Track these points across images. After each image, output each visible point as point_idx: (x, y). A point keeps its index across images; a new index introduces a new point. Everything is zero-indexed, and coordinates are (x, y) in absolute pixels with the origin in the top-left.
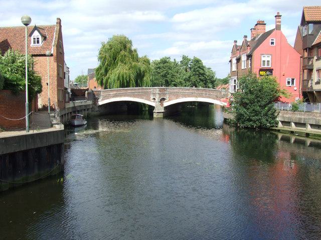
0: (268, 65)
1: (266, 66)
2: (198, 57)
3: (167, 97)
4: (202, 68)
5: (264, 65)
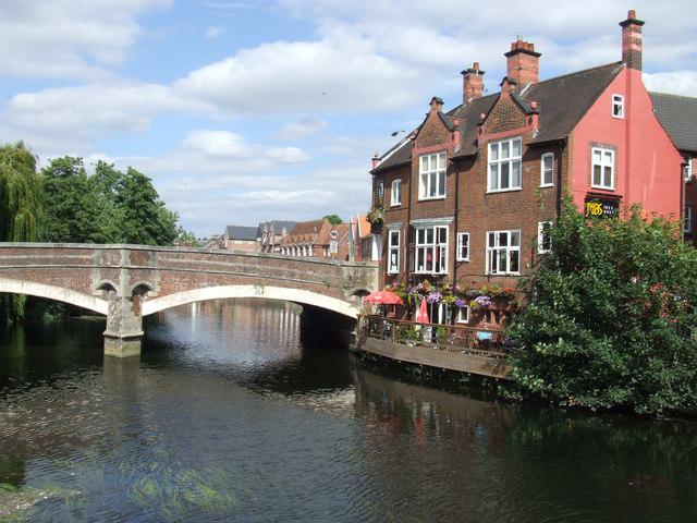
0: (608, 182)
1: (602, 186)
2: (142, 170)
3: (154, 281)
4: (149, 197)
5: (597, 181)
